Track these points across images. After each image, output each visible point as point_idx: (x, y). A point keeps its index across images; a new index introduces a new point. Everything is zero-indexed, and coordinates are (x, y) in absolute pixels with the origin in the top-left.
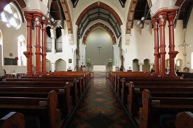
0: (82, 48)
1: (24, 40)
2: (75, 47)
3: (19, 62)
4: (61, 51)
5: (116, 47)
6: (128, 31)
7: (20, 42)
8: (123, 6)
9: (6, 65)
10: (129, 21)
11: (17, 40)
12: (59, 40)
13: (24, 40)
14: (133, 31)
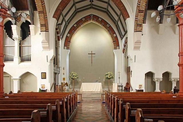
2: (51, 53)
4: (29, 60)
6: (138, 27)
10: (140, 11)
12: (25, 44)
14: (146, 27)
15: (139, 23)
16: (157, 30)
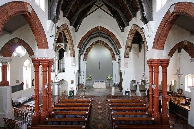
0: (84, 64)
1: (29, 63)
2: (76, 69)
3: (25, 87)
4: (63, 71)
5: (115, 63)
6: (127, 55)
7: (26, 67)
8: (123, 31)
9: (13, 93)
10: (128, 47)
11: (24, 65)
12: (61, 62)
13: (29, 63)
14: (131, 54)
15: (127, 53)
16: (138, 56)
